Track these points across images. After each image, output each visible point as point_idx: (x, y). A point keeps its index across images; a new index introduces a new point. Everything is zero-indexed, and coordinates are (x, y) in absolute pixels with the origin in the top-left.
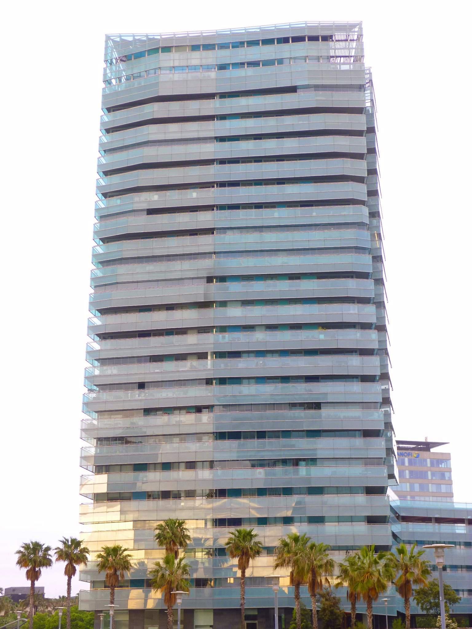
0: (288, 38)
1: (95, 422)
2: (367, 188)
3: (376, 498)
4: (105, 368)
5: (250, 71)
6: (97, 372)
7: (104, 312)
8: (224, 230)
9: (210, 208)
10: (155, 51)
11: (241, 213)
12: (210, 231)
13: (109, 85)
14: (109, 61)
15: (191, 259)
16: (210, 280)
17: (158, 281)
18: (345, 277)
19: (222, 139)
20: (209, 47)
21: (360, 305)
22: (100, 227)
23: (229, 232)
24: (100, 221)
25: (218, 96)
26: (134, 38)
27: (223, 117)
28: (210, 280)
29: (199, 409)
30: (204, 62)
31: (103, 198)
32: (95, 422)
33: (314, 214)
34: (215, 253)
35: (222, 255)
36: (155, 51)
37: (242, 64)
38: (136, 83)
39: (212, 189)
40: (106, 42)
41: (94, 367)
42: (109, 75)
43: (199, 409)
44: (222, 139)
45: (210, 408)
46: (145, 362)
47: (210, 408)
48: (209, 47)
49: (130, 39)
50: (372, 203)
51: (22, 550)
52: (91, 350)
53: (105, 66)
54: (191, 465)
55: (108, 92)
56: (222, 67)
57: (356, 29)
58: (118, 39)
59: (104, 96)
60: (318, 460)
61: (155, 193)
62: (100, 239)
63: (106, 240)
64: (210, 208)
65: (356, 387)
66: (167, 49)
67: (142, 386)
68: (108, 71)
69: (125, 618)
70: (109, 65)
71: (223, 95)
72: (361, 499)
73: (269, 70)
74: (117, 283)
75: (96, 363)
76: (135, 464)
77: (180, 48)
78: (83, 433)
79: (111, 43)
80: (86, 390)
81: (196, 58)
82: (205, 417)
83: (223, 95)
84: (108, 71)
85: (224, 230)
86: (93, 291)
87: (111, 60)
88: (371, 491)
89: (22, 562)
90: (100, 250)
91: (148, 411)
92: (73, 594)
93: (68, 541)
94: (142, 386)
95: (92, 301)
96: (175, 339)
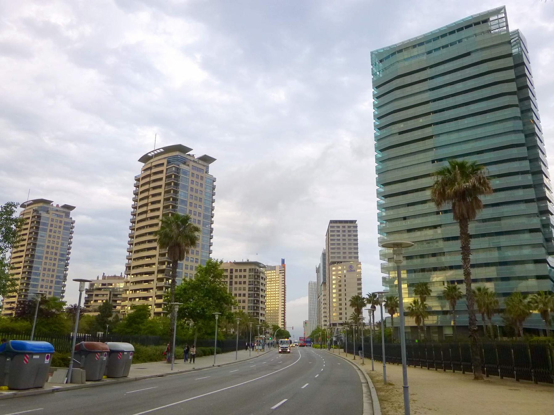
0: (455, 31)
1: (385, 238)
2: (518, 98)
3: (540, 266)
4: (387, 212)
5: (444, 51)
6: (384, 214)
7: (385, 185)
8: (439, 135)
9: (430, 125)
10: (394, 54)
11: (447, 124)
12: (431, 137)
13: (375, 76)
14: (375, 64)
15: (408, 156)
16: (433, 162)
17: (424, 162)
18: (510, 148)
19: (433, 89)
20: (421, 44)
21: (520, 162)
22: (378, 145)
23: (441, 136)
24: (378, 142)
25: (429, 68)
26: (384, 50)
27: (432, 78)
28: (433, 162)
29: (435, 227)
30: (420, 52)
31: (379, 130)
32: (385, 238)
33: (488, 117)
34: (434, 148)
35: (462, 143)
36: (394, 54)
37: (440, 48)
38: (387, 71)
39: (430, 116)
40: (371, 55)
41: (382, 212)
42: (375, 71)
43: (435, 227)
44: (433, 89)
45: (440, 226)
46: (405, 207)
47: (440, 226)
48: (421, 44)
49: (382, 51)
50: (527, 104)
51: (352, 299)
52: (380, 204)
53: (372, 67)
54: (422, 256)
55: (375, 79)
56: (429, 52)
57: (503, 11)
58: (376, 53)
59: (373, 82)
60: (501, 248)
61: (401, 123)
62: (379, 150)
63: (381, 151)
64: (430, 125)
65: (523, 206)
66: (400, 51)
67: (405, 218)
68: (374, 69)
69: (409, 330)
70: (374, 66)
71: (431, 67)
72: (531, 267)
73: (454, 47)
74: (388, 170)
75: (384, 210)
76: (432, 254)
77: (407, 48)
78: (380, 244)
79: (374, 56)
80: (379, 223)
81: (415, 52)
82: (439, 230)
83: (431, 67)
84: (374, 69)
85: (439, 135)
86: (377, 176)
87: (376, 63)
88: (537, 262)
89: (352, 305)
90: (379, 156)
91: (409, 231)
92: (384, 319)
93: (370, 294)
94: (405, 218)
95: (377, 181)
96: (420, 193)
